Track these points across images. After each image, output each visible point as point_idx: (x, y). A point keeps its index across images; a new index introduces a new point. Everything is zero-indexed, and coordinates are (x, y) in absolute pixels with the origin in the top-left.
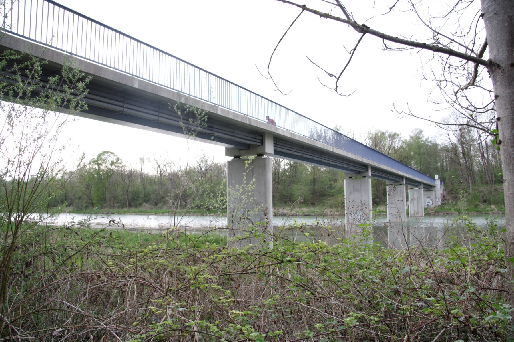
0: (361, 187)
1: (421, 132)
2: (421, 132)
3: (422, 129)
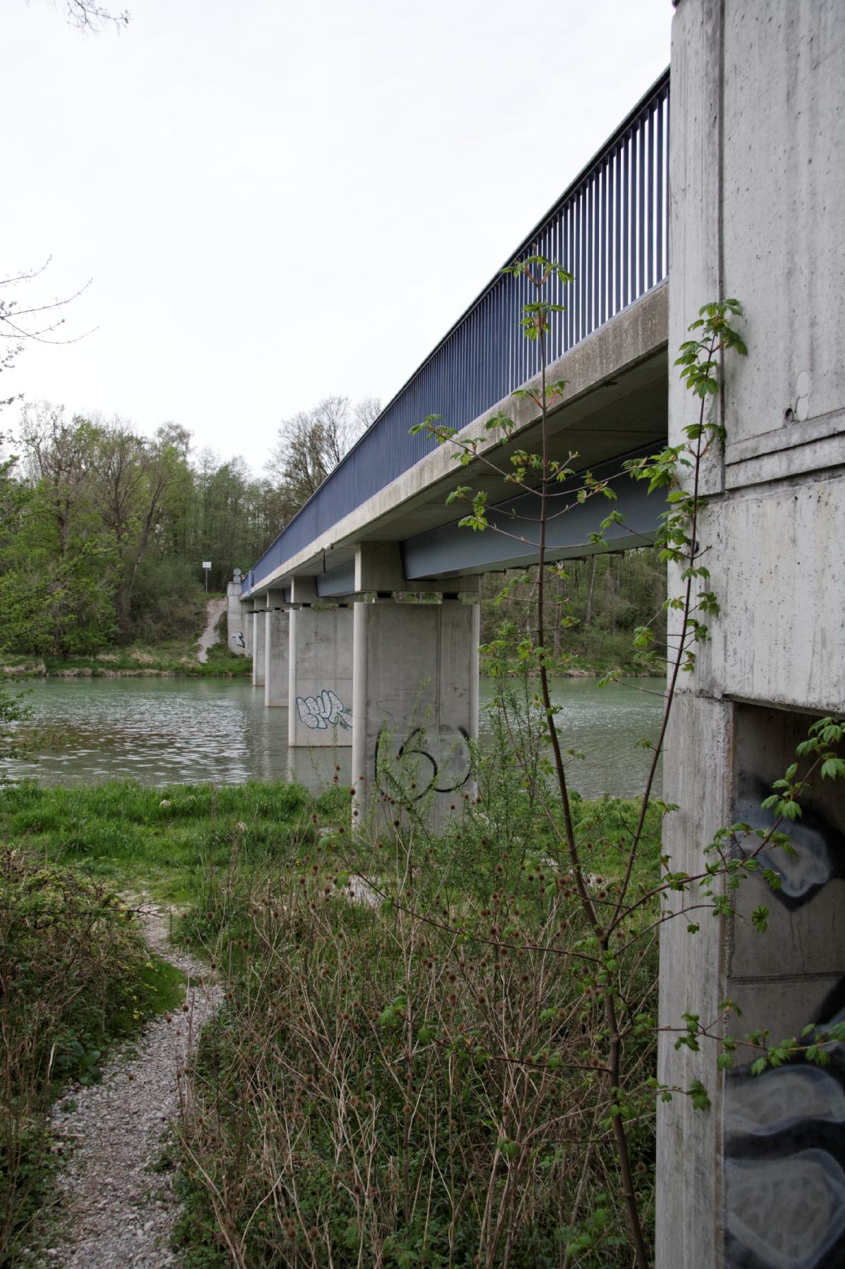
0: (336, 631)
1: (183, 437)
2: (183, 437)
3: (187, 427)
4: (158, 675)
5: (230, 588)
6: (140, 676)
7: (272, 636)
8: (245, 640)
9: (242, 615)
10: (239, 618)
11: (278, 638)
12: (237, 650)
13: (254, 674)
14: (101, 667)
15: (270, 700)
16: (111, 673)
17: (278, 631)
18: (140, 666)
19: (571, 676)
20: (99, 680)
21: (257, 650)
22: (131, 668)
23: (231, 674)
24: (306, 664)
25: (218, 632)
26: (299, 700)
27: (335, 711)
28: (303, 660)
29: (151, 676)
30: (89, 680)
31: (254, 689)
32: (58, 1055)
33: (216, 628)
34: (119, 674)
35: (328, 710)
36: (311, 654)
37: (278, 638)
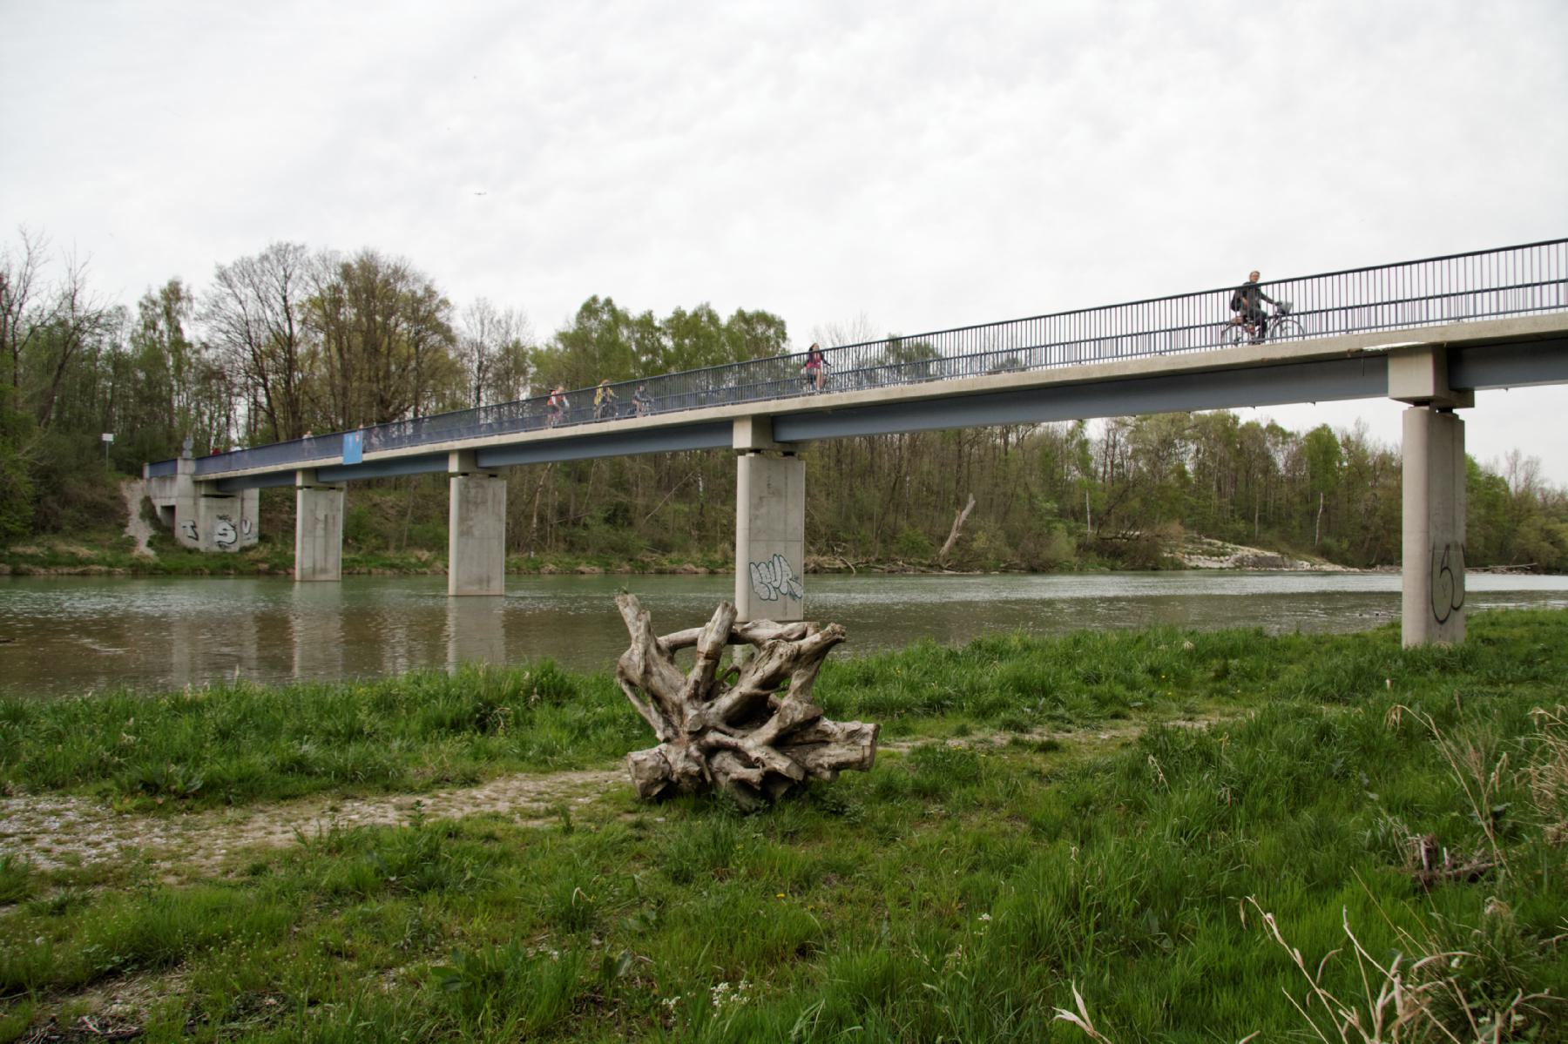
4: (109, 574)
5: (180, 463)
6: (84, 574)
7: (460, 507)
8: (199, 530)
9: (195, 499)
10: (191, 502)
11: (468, 510)
12: (190, 543)
13: (298, 567)
14: (27, 562)
15: (458, 587)
16: (42, 571)
17: (468, 502)
18: (81, 562)
19: (582, 573)
20: (23, 580)
21: (303, 536)
22: (68, 565)
23: (207, 571)
24: (759, 523)
25: (148, 522)
26: (753, 566)
27: (785, 579)
28: (757, 517)
29: (100, 574)
30: (8, 579)
31: (297, 585)
32: (1467, 1029)
33: (142, 516)
34: (52, 571)
35: (779, 578)
36: (763, 510)
37: (468, 510)
